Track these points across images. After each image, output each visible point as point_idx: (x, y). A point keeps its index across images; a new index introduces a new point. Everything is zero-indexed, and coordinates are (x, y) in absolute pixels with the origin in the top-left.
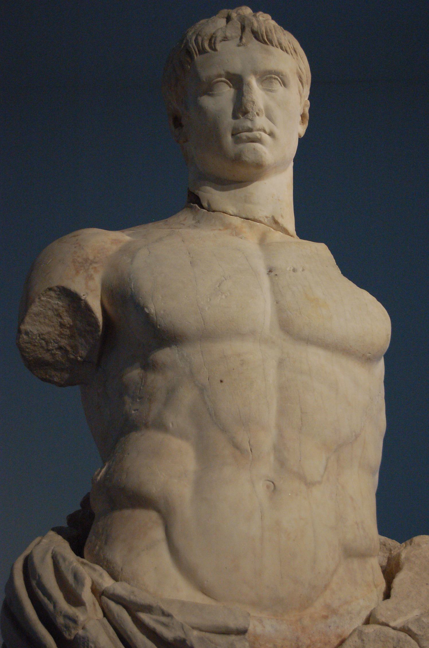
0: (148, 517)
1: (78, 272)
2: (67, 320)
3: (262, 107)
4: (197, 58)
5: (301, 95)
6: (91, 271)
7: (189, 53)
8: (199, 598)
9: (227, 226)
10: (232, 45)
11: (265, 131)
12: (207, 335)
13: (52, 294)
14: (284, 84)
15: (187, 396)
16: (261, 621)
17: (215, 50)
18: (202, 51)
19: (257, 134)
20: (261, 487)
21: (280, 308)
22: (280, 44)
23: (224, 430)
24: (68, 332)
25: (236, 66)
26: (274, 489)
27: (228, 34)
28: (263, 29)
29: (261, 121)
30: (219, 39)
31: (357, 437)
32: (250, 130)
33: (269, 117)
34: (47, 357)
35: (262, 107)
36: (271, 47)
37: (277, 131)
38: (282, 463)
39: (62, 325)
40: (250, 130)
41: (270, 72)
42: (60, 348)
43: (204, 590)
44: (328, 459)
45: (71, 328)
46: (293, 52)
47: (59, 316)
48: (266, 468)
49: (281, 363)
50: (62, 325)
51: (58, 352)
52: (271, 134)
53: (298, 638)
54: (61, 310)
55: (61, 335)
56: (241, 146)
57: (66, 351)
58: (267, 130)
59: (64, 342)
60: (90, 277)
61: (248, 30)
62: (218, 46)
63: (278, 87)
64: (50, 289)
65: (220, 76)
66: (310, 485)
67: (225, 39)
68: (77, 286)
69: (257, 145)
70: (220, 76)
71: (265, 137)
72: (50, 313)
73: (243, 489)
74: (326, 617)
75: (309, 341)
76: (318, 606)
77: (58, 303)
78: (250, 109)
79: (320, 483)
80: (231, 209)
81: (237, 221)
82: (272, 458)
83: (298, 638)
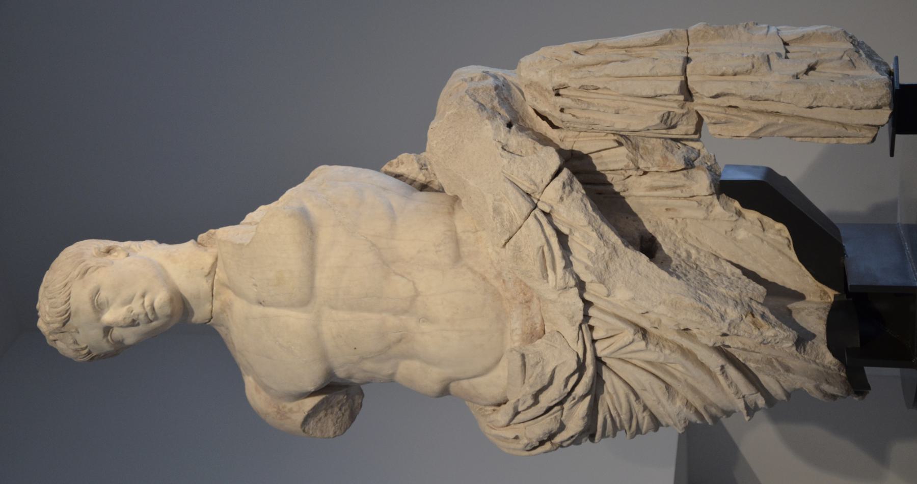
0: (453, 385)
1: (289, 418)
2: (322, 414)
3: (125, 309)
4: (94, 354)
5: (98, 268)
6: (286, 410)
7: (92, 359)
8: (504, 363)
9: (223, 311)
10: (79, 338)
11: (143, 303)
12: (324, 356)
13: (306, 429)
14: (98, 291)
15: (369, 365)
16: (513, 331)
17: (86, 347)
18: (89, 353)
19: (148, 309)
20: (425, 327)
21: (291, 306)
22: (66, 302)
23: (389, 347)
24: (329, 411)
25: (97, 333)
26: (426, 319)
27: (72, 341)
28: (59, 319)
29: (136, 308)
30: (77, 347)
31: (373, 245)
32: (146, 315)
33: (130, 301)
34: (347, 413)
35: (125, 309)
36: (73, 309)
37: (139, 293)
38: (405, 311)
39: (326, 415)
40: (146, 315)
41: (94, 307)
42: (340, 409)
43: (498, 361)
44: (397, 274)
45: (326, 410)
46: (67, 288)
47: (320, 420)
48: (411, 322)
49: (333, 308)
50: (326, 415)
51: (343, 409)
52: (143, 296)
53: (521, 303)
54: (316, 420)
55: (332, 413)
56: (159, 315)
57: (342, 405)
58: (141, 301)
59: (336, 409)
60: (291, 410)
61: (63, 330)
62: (84, 346)
63: (103, 295)
64: (304, 431)
65: (108, 341)
66: (417, 294)
67: (76, 342)
68: (299, 418)
69: (156, 305)
70: (108, 341)
71: (147, 303)
72: (319, 425)
73: (429, 338)
74: (504, 281)
75: (312, 287)
76: (497, 284)
77: (312, 423)
78: (130, 320)
79: (414, 284)
80: (208, 307)
81: (217, 305)
82: (403, 317)
83: (521, 303)
